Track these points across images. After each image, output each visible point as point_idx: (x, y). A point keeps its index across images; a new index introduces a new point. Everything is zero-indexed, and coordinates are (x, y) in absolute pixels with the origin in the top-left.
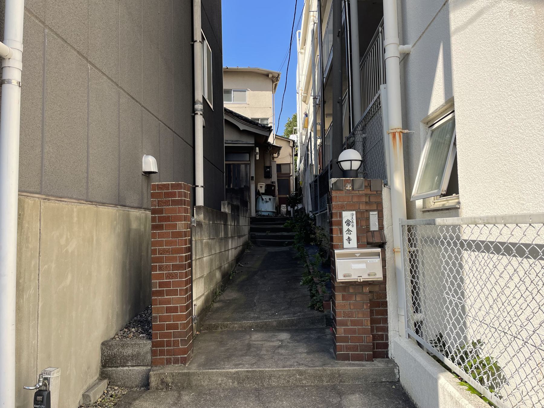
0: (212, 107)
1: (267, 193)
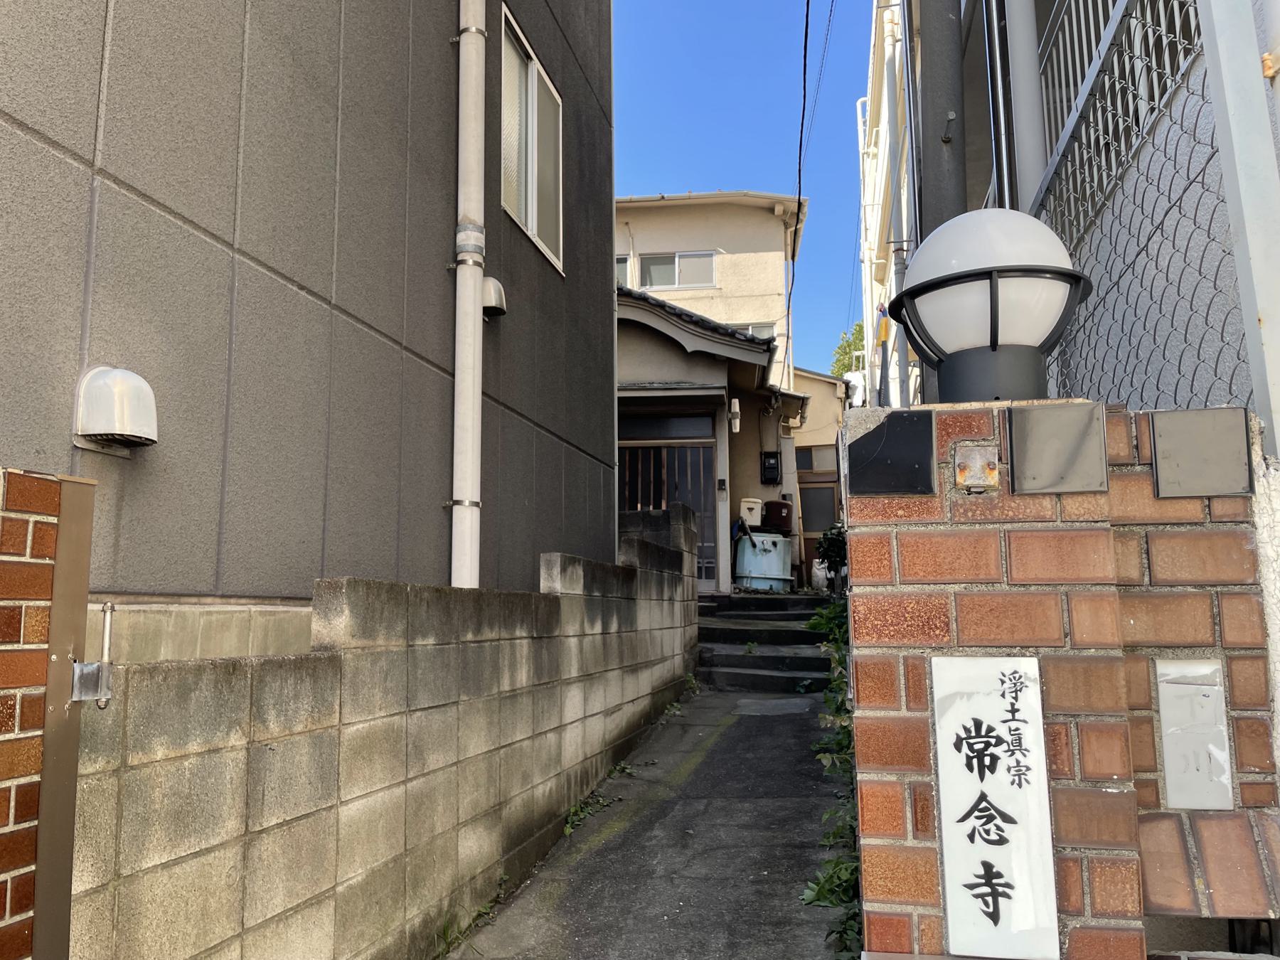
0: (559, 265)
1: (765, 527)
